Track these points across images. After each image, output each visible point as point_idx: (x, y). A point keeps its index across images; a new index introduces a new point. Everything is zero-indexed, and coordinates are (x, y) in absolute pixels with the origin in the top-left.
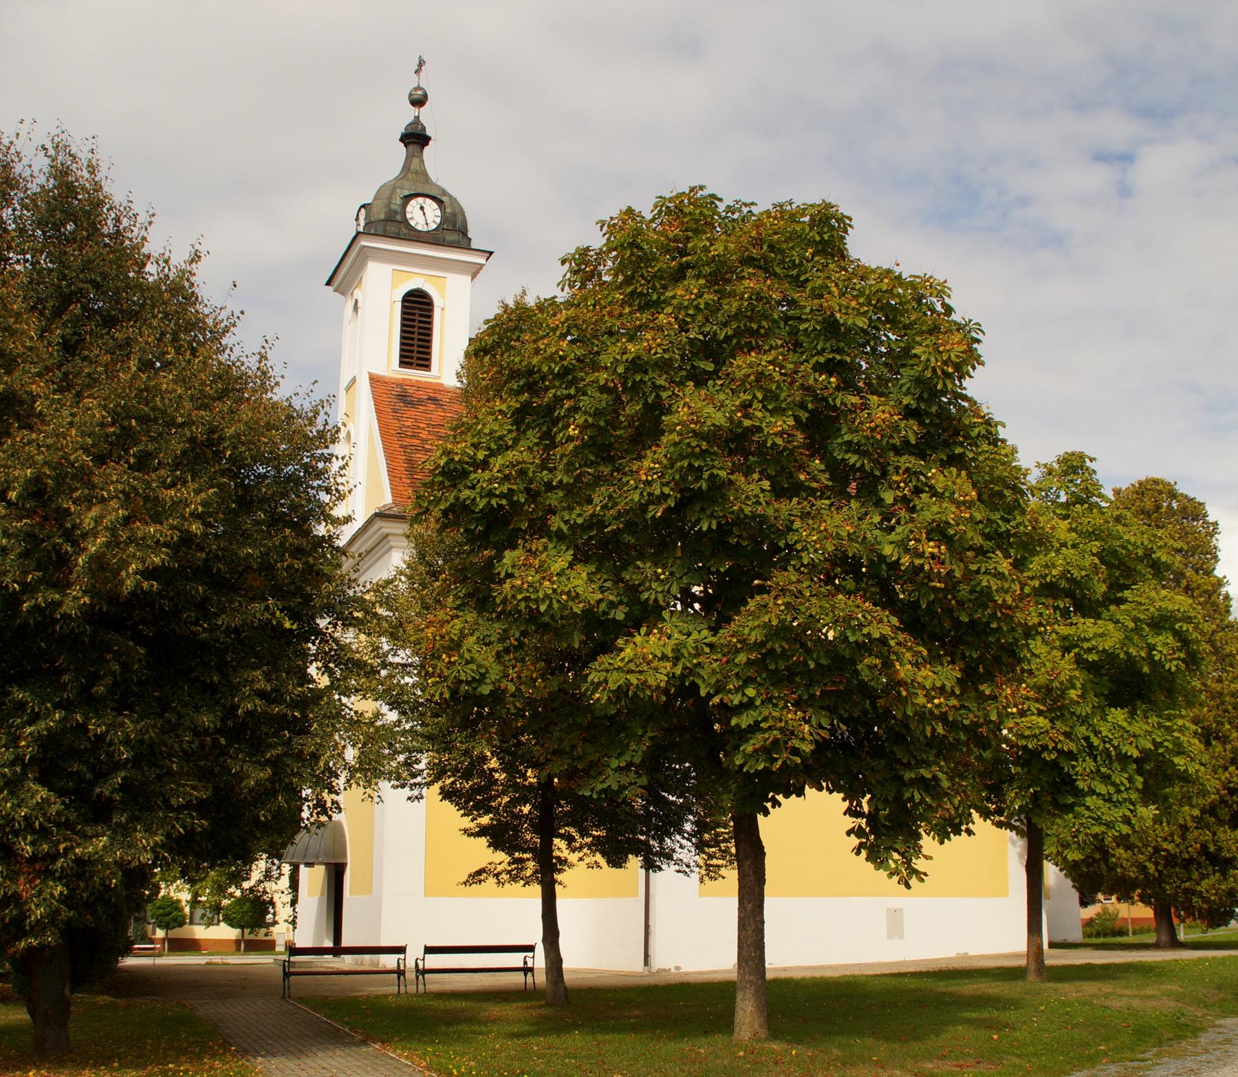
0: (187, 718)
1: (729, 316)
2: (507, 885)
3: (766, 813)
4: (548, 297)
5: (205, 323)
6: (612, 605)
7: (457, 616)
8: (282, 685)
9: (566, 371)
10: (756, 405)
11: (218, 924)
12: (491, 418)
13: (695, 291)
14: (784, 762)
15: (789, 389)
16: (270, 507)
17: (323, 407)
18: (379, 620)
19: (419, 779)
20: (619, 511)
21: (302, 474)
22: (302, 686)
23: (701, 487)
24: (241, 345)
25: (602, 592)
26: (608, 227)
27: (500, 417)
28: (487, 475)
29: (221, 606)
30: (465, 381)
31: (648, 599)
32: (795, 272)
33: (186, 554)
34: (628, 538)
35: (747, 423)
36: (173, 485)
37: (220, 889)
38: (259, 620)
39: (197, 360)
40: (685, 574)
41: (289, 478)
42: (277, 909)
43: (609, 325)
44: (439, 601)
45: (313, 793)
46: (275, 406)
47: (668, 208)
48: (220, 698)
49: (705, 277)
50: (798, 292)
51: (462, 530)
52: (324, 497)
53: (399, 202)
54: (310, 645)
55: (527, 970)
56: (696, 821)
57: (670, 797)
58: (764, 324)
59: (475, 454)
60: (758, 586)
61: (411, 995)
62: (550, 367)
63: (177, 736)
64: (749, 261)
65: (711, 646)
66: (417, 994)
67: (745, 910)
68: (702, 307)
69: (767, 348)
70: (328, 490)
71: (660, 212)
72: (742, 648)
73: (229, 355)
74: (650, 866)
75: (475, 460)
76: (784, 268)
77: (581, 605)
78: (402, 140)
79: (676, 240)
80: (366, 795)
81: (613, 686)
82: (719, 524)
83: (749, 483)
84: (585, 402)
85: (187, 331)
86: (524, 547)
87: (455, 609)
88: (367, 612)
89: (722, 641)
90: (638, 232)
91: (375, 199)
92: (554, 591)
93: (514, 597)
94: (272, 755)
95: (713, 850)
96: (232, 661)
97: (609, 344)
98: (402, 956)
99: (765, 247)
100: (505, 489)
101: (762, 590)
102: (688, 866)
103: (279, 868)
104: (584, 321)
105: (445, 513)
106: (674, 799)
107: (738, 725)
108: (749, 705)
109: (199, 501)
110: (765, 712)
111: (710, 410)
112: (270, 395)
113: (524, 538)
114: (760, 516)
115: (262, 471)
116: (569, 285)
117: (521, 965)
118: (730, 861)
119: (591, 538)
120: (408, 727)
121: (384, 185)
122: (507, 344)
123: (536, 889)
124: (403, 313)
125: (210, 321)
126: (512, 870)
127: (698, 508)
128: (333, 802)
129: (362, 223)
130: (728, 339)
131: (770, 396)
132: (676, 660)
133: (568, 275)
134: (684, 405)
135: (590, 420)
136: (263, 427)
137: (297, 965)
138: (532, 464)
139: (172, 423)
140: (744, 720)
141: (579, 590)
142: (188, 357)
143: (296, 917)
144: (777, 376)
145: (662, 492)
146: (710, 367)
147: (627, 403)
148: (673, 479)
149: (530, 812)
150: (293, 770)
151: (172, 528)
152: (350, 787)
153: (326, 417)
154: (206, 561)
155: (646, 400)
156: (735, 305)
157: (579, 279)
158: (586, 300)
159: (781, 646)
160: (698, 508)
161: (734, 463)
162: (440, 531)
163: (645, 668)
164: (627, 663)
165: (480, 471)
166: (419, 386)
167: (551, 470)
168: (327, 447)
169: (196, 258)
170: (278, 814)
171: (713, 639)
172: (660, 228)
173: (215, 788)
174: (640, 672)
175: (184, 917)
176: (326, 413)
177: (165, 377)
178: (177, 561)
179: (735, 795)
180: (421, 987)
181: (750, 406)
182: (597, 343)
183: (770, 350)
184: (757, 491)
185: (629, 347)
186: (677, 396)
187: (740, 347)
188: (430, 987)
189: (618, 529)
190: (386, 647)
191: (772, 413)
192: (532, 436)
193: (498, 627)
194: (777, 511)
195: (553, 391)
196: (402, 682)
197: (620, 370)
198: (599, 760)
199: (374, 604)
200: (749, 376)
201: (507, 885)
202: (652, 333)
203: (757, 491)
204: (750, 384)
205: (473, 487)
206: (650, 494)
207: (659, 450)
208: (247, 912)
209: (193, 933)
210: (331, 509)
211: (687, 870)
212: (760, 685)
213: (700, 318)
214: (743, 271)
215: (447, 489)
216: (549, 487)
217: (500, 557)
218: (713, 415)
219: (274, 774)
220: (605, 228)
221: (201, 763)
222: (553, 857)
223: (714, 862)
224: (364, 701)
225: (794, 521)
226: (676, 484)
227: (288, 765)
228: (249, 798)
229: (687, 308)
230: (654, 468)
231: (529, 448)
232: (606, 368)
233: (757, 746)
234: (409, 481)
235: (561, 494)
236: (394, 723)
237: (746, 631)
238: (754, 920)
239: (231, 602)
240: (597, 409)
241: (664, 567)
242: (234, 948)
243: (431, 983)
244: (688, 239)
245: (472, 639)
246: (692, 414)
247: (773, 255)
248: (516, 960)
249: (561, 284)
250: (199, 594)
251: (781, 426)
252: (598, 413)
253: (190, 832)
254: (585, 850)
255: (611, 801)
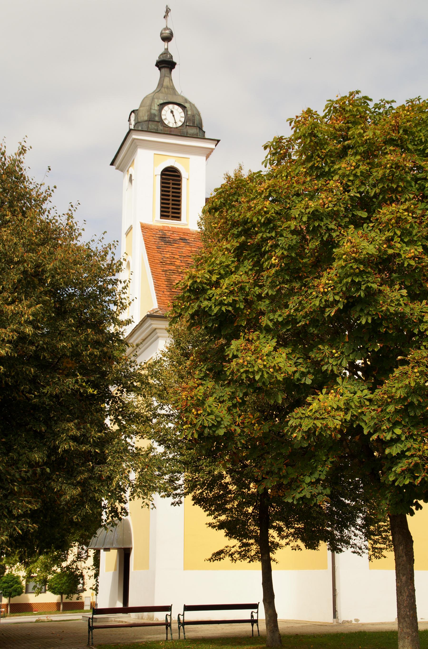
0: (24, 455)
1: (377, 180)
2: (238, 561)
3: (412, 514)
4: (256, 171)
5: (30, 195)
6: (303, 374)
7: (202, 384)
8: (87, 432)
9: (269, 221)
10: (396, 239)
11: (45, 592)
12: (220, 253)
13: (354, 164)
14: (423, 479)
15: (419, 228)
16: (77, 315)
17: (110, 249)
18: (151, 387)
19: (178, 491)
20: (306, 312)
21: (98, 293)
22: (100, 432)
23: (360, 295)
24: (55, 208)
25: (296, 366)
26: (295, 123)
27: (226, 253)
28: (219, 291)
29: (47, 381)
30: (203, 228)
31: (327, 370)
32: (422, 147)
33: (23, 348)
34: (312, 330)
35: (390, 251)
36: (13, 302)
37: (47, 568)
38: (72, 389)
39: (26, 220)
40: (351, 353)
41: (90, 296)
42: (85, 581)
43: (296, 189)
44: (190, 372)
45: (109, 503)
46: (79, 249)
47: (335, 108)
48: (46, 441)
49: (360, 154)
50: (424, 161)
51: (203, 327)
52: (113, 307)
53: (156, 108)
54: (106, 405)
55: (253, 621)
56: (364, 518)
57: (347, 502)
58: (401, 184)
59: (210, 278)
60: (400, 360)
61: (175, 640)
62: (258, 219)
63: (18, 468)
64: (390, 141)
65: (370, 400)
66: (179, 640)
67: (401, 581)
68: (359, 174)
69: (403, 200)
70: (115, 303)
71: (329, 111)
72: (391, 402)
73: (48, 216)
74: (334, 549)
75: (210, 281)
76: (414, 145)
77: (282, 375)
78: (157, 65)
79: (341, 130)
80: (144, 504)
81: (306, 429)
82: (373, 319)
83: (393, 292)
84: (282, 241)
85: (19, 200)
86: (244, 337)
87: (200, 379)
88: (142, 383)
89: (377, 397)
90: (315, 126)
91: (141, 106)
92: (265, 366)
93: (238, 370)
94: (81, 479)
95: (377, 537)
96: (54, 417)
97: (297, 202)
98: (169, 613)
99: (401, 131)
100: (230, 300)
101: (405, 362)
102: (360, 549)
103: (87, 551)
104: (280, 187)
105: (192, 316)
106: (349, 502)
107: (390, 454)
108: (397, 440)
109: (30, 312)
110: (409, 445)
111: (365, 244)
112: (75, 242)
113: (244, 331)
114: (401, 313)
115: (71, 291)
116: (270, 163)
117: (249, 618)
118: (389, 545)
119: (288, 330)
120: (171, 456)
121: (146, 97)
122: (230, 204)
123: (258, 565)
124: (162, 183)
125: (34, 193)
126: (242, 552)
127: (358, 309)
128: (122, 509)
129: (133, 123)
130: (376, 196)
131: (406, 233)
132: (347, 410)
133: (269, 157)
134: (348, 241)
135: (285, 253)
136: (72, 263)
137: (98, 620)
138: (248, 283)
139: (11, 261)
140: (394, 450)
141: (281, 365)
142: (20, 218)
143: (98, 585)
144: (410, 219)
145: (334, 299)
146: (364, 215)
147: (310, 241)
148: (342, 290)
149: (253, 512)
150: (95, 488)
151: (13, 331)
152: (134, 498)
153: (113, 255)
154: (35, 351)
155: (322, 238)
156: (381, 172)
157: (276, 159)
158: (281, 172)
159: (418, 400)
160: (358, 309)
161: (382, 279)
162: (189, 328)
163: (326, 416)
164: (314, 413)
165: (214, 288)
166: (174, 231)
167: (261, 287)
168: (114, 275)
169: (23, 151)
170: (86, 517)
171: (371, 396)
172: (329, 122)
173: (43, 501)
174: (322, 419)
175: (22, 588)
176: (113, 253)
177: (5, 231)
178: (16, 352)
179: (390, 501)
180: (182, 634)
181: (392, 240)
182: (288, 201)
183: (405, 202)
184: (398, 297)
185: (310, 204)
186: (343, 235)
187: (384, 201)
188: (189, 635)
189: (306, 324)
190: (156, 404)
191: (407, 244)
192: (248, 265)
193: (228, 390)
194: (412, 309)
195: (261, 234)
196: (167, 427)
197: (305, 219)
198: (297, 477)
199: (147, 377)
200: (391, 220)
201: (238, 561)
202: (326, 194)
203: (398, 297)
204: (392, 225)
205: (210, 299)
206: (326, 301)
207: (332, 271)
208: (65, 583)
209: (28, 599)
210: (118, 315)
211: (360, 551)
212: (404, 426)
213: (357, 182)
214: (386, 148)
215: (193, 301)
216: (259, 297)
217: (228, 344)
218: (368, 247)
219: (83, 491)
220: (293, 124)
221: (34, 486)
222: (268, 542)
223: (378, 546)
224: (142, 440)
225: (424, 316)
226: (343, 294)
227: (92, 485)
228: (66, 508)
229: (348, 176)
230: (328, 284)
231: (246, 272)
232: (295, 218)
233: (404, 468)
234: (169, 293)
235: (267, 302)
236: (162, 454)
237: (394, 390)
238: (408, 589)
239: (53, 378)
240: (290, 245)
241: (337, 348)
242: (55, 609)
243: (190, 631)
244: (349, 128)
245: (211, 399)
246: (353, 247)
247: (406, 137)
248: (245, 614)
249: (265, 163)
250: (31, 373)
251: (413, 252)
252: (291, 248)
253: (26, 533)
254: (290, 538)
255: (306, 505)
